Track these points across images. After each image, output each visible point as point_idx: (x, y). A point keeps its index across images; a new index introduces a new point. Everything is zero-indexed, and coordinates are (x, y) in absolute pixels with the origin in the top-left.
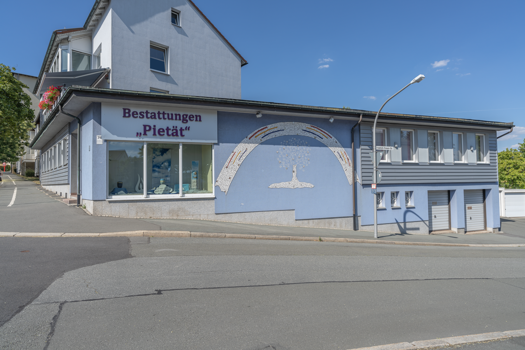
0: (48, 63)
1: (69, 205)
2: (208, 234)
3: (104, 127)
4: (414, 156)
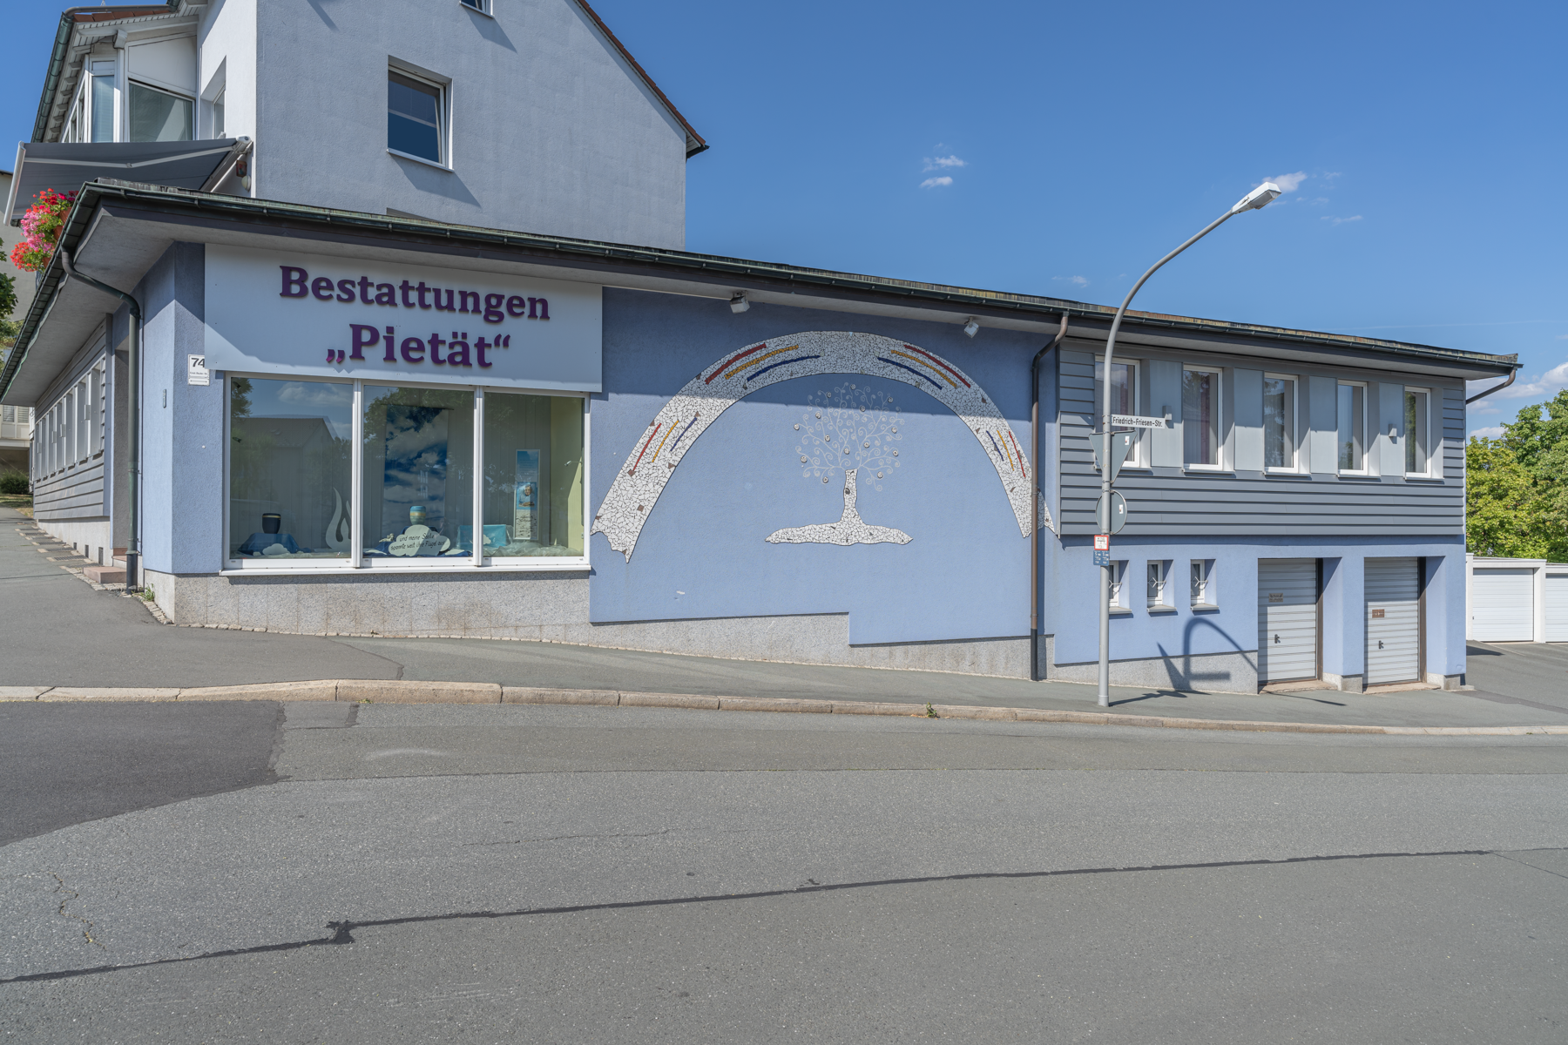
0: (52, 123)
1: (98, 587)
2: (560, 694)
3: (215, 326)
4: (1220, 450)
